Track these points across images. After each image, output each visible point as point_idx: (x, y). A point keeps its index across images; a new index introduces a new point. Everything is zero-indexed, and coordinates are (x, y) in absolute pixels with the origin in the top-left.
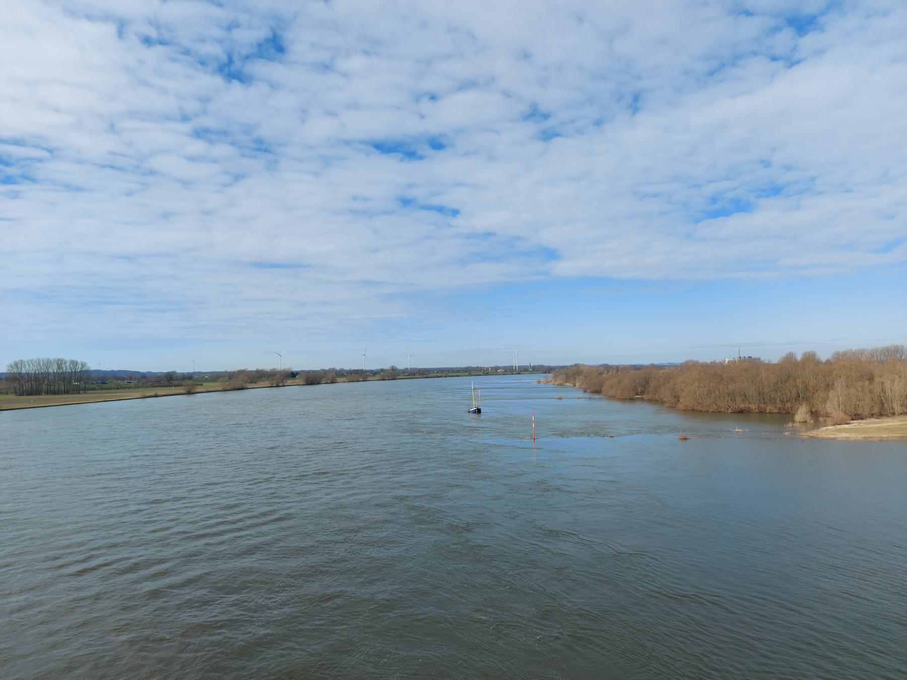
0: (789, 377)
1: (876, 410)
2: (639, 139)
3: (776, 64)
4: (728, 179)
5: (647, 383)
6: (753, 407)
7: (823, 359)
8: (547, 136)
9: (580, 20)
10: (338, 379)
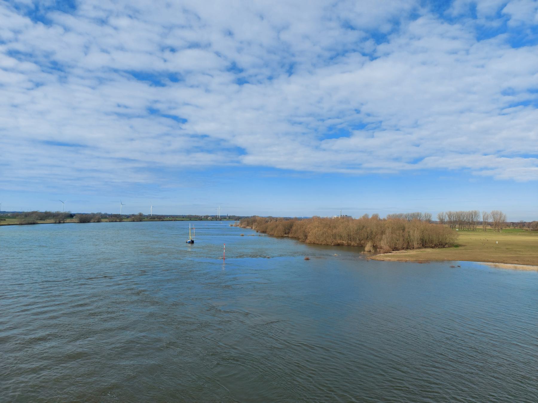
0: (364, 227)
1: (405, 246)
2: (293, 91)
3: (364, 58)
4: (338, 118)
5: (291, 227)
6: (344, 242)
7: (357, 218)
8: (241, 82)
9: (262, 17)
10: (102, 220)
